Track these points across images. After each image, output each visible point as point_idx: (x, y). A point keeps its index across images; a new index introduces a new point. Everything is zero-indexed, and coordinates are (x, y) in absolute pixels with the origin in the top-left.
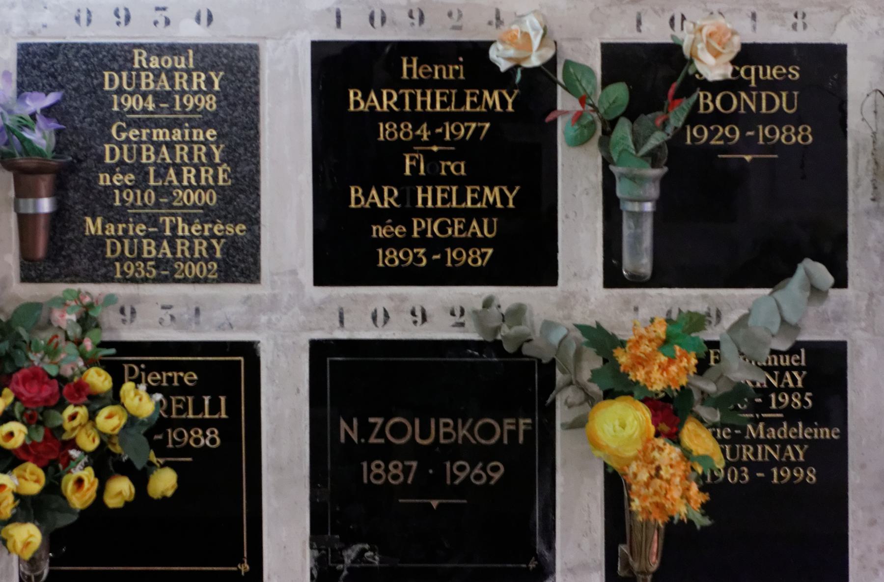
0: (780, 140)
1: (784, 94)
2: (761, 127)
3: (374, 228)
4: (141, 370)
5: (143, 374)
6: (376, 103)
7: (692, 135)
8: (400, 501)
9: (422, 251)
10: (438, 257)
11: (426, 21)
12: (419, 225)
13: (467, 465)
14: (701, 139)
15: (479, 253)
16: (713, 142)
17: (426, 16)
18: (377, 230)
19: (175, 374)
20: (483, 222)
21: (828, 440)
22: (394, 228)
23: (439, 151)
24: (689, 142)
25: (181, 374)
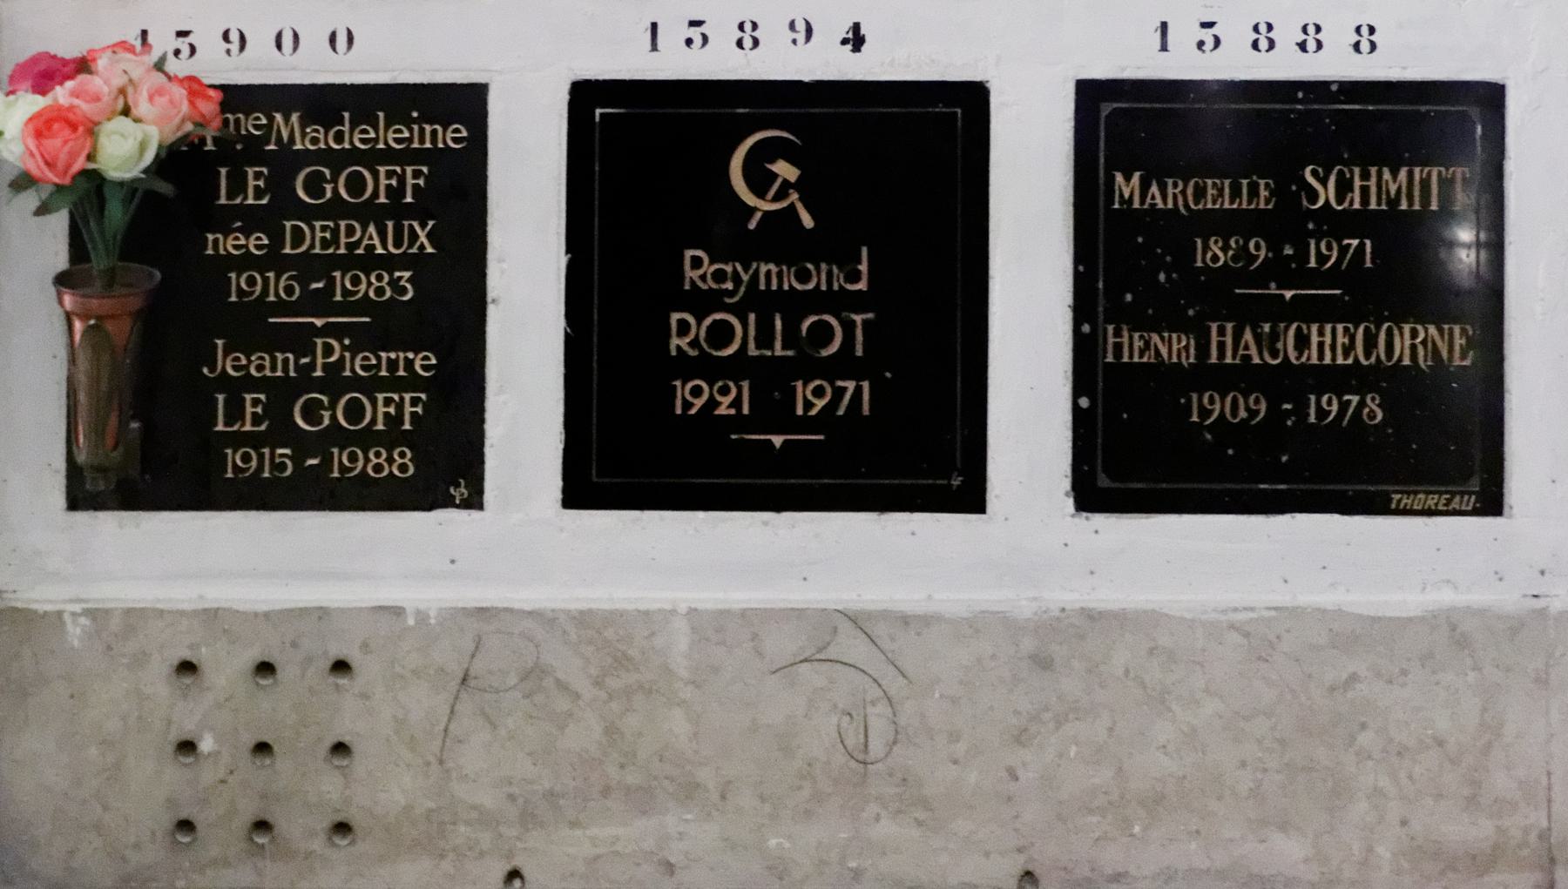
3: (210, 237)
4: (344, 348)
5: (347, 355)
6: (376, 241)
9: (407, 274)
13: (825, 384)
18: (216, 241)
19: (402, 355)
21: (823, 261)
22: (247, 238)
23: (1098, 289)
25: (411, 355)
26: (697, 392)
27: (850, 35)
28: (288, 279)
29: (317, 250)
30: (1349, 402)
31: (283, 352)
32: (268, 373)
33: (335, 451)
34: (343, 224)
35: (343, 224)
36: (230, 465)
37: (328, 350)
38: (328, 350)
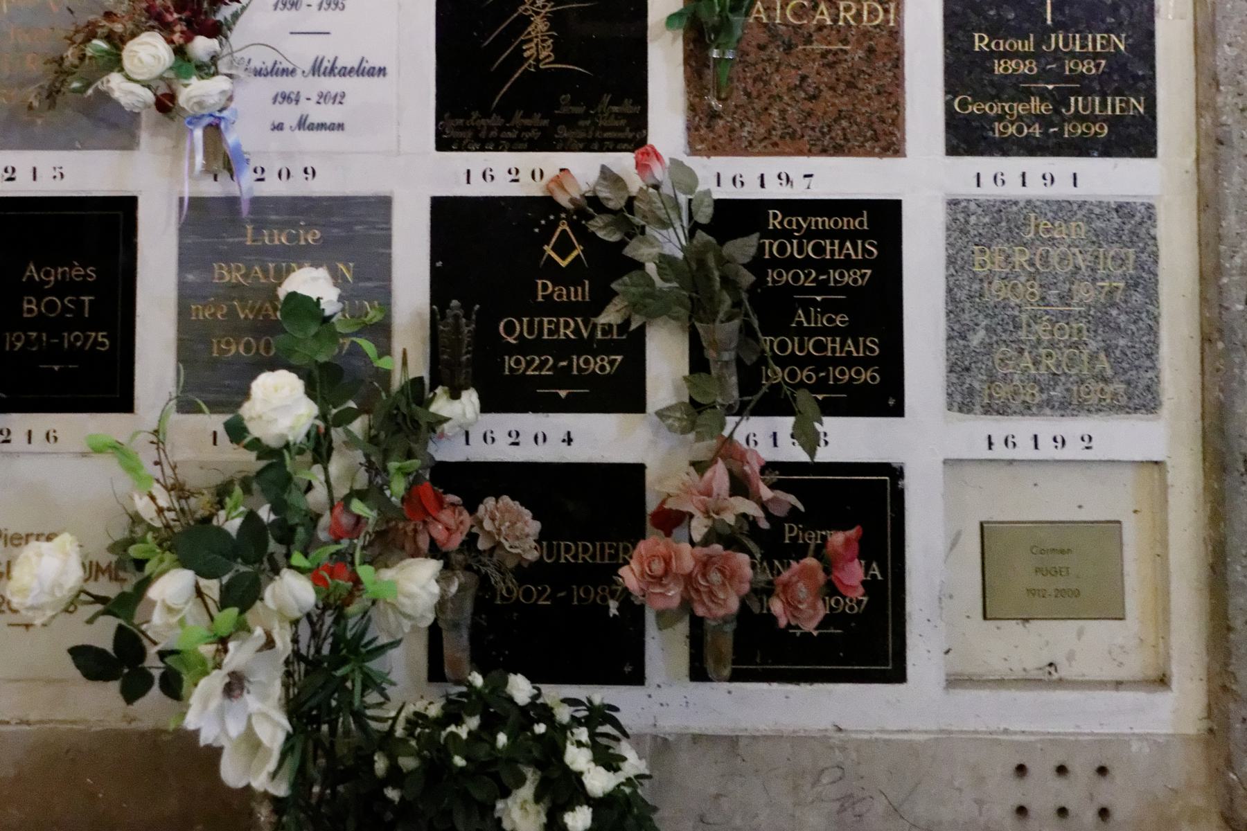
0: (594, 370)
1: (796, 339)
2: (831, 368)
4: (799, 528)
6: (851, 252)
7: (834, 375)
8: (87, 316)
10: (564, 363)
11: (482, 435)
12: (545, 287)
13: (21, 333)
14: (518, 370)
15: (859, 273)
16: (528, 373)
17: (482, 439)
20: (858, 342)
24: (507, 372)
26: (77, 338)
27: (566, 438)
28: (859, 380)
29: (546, 337)
30: (90, 336)
31: (578, 301)
32: (598, 561)
33: (831, 271)
34: (562, 320)
35: (562, 320)
36: (507, 366)
37: (791, 530)
38: (791, 530)
